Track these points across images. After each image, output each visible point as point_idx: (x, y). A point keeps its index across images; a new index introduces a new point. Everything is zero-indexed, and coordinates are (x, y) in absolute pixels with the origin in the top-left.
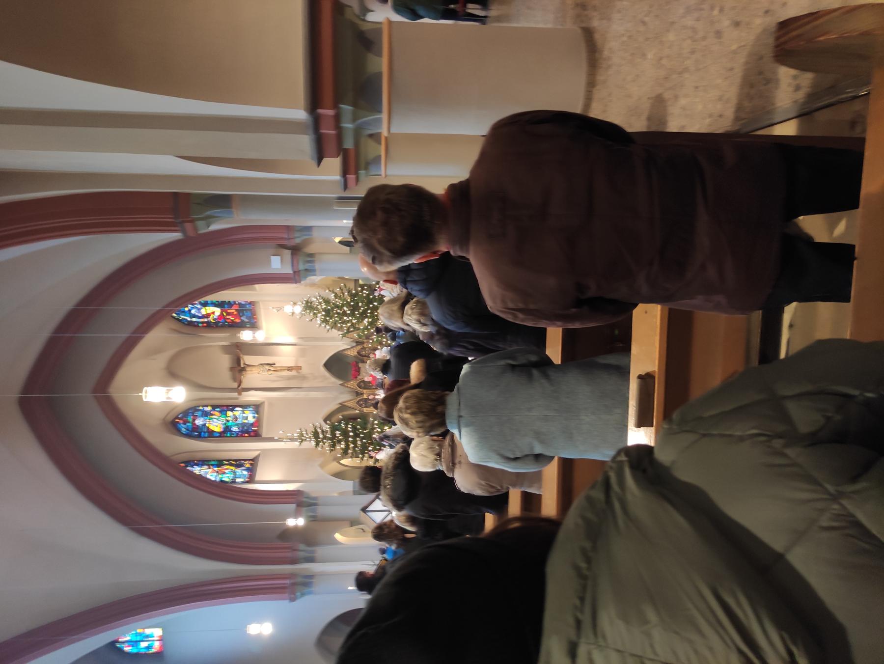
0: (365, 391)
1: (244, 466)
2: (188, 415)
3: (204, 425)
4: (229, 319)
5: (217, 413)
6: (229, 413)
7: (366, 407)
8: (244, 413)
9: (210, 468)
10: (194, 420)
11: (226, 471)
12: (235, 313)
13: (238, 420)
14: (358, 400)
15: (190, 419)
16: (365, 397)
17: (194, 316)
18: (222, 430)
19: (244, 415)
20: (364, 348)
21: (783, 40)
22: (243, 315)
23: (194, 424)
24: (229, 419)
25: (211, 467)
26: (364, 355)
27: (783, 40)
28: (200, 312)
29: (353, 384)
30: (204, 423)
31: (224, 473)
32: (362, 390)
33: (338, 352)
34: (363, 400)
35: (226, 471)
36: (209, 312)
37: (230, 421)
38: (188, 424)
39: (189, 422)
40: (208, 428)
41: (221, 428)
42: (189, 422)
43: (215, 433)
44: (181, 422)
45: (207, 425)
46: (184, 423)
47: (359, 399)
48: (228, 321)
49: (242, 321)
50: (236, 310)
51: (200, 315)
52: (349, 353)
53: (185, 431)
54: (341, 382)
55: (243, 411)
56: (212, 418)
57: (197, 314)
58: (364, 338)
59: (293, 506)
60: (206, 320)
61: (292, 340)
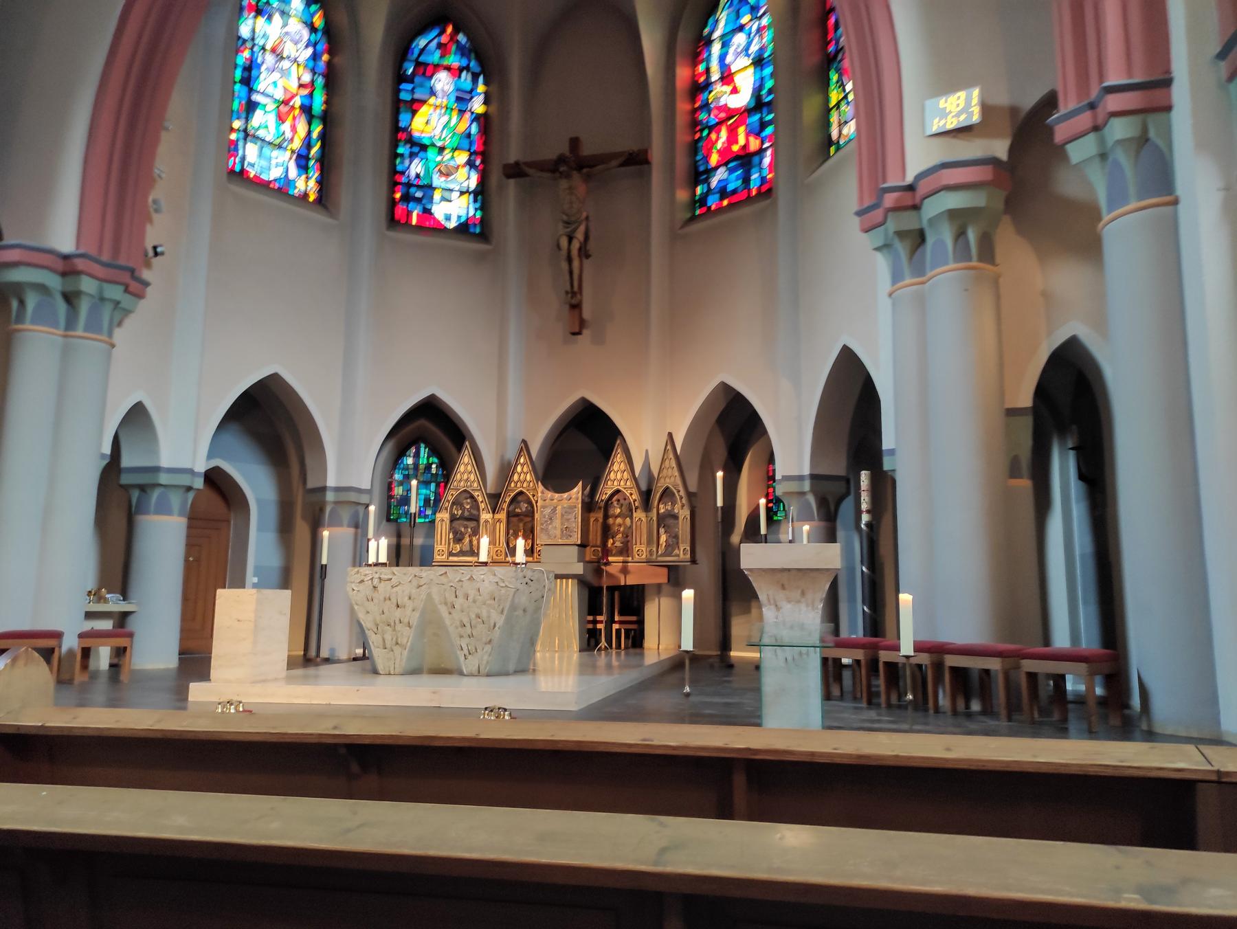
0: (502, 516)
1: (300, 175)
2: (463, 55)
3: (433, 93)
4: (718, 138)
5: (463, 127)
6: (462, 157)
7: (453, 519)
8: (462, 193)
9: (301, 86)
10: (448, 68)
11: (286, 127)
12: (735, 148)
13: (443, 179)
14: (475, 494)
15: (453, 60)
16: (485, 516)
17: (725, 44)
18: (416, 134)
19: (455, 195)
20: (630, 510)
21: (772, 601)
22: (731, 171)
23: (437, 68)
24: (447, 154)
25: (306, 92)
26: (611, 512)
27: (772, 601)
28: (738, 55)
29: (524, 477)
30: (440, 94)
31: (281, 119)
32: (505, 506)
33: (764, 432)
34: (475, 512)
35: (286, 127)
36: (738, 80)
37: (439, 158)
38: (437, 54)
39: (442, 56)
40: (423, 102)
41: (422, 132)
42: (442, 56)
43: (409, 115)
44: (444, 39)
45: (432, 100)
46: (440, 46)
47: (480, 499)
48: (713, 136)
49: (711, 171)
50: (746, 146)
51: (729, 59)
52: (616, 467)
53: (418, 45)
54: (535, 450)
55: (467, 191)
56: (450, 114)
57: (731, 50)
58: (662, 511)
59: (771, 466)
60: (715, 76)
61: (657, 600)
